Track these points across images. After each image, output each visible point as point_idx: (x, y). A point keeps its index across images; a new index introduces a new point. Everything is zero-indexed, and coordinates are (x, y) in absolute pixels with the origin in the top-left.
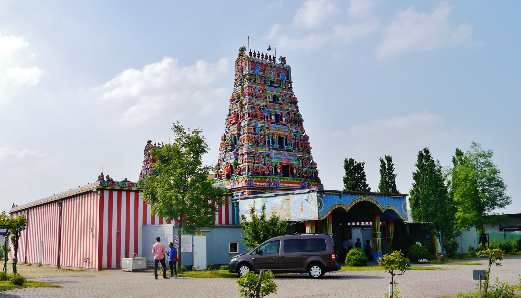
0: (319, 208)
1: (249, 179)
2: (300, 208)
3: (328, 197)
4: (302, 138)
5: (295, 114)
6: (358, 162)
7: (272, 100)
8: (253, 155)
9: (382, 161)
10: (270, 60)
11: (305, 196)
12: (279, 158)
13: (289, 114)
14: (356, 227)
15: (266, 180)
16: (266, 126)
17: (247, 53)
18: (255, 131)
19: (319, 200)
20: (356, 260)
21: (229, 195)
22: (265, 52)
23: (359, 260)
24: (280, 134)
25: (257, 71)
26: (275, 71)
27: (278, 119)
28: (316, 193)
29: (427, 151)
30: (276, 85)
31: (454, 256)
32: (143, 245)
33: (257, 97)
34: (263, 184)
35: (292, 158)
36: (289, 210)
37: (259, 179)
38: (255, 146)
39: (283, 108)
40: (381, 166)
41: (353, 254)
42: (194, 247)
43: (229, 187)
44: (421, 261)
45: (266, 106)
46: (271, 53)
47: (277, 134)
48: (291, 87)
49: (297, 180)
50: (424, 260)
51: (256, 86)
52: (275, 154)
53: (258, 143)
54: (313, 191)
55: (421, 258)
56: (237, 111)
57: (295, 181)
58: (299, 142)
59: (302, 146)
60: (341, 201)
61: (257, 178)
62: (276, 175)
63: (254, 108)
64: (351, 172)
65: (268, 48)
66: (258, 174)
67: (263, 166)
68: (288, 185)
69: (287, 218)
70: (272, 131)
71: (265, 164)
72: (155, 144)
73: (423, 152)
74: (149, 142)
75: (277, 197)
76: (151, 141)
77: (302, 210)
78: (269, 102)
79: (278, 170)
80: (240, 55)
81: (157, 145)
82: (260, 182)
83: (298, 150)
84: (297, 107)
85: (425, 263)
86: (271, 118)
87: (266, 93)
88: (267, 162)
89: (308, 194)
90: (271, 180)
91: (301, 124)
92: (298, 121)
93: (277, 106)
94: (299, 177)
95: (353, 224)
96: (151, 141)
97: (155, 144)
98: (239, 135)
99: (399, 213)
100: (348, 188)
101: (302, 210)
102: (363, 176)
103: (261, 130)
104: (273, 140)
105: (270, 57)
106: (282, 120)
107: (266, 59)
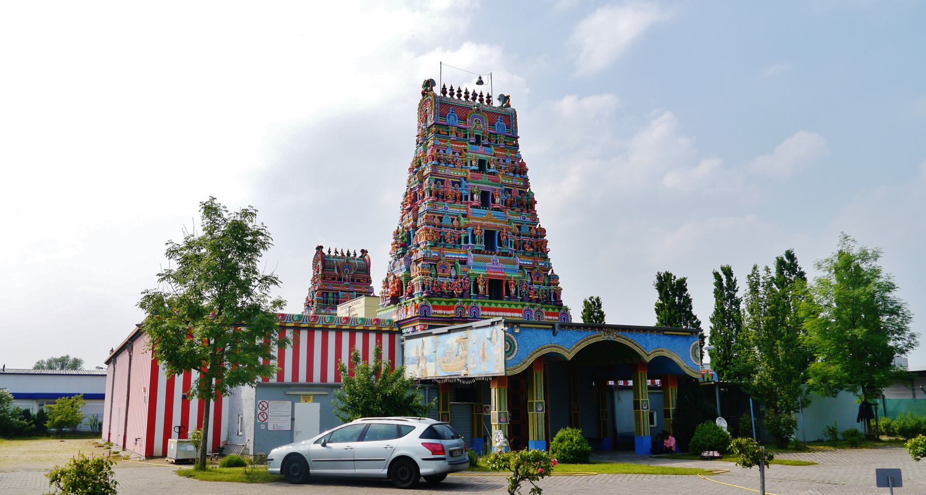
0: (508, 353)
1: (423, 303)
2: (481, 352)
3: (527, 333)
4: (533, 232)
5: (521, 192)
6: (678, 278)
7: (477, 168)
8: (432, 264)
9: (716, 275)
10: (481, 100)
11: (487, 331)
12: (483, 267)
13: (510, 191)
14: (626, 388)
15: (447, 304)
16: (464, 212)
17: (437, 90)
18: (441, 221)
19: (507, 339)
20: (564, 451)
21: (397, 332)
22: (472, 87)
23: (571, 452)
24: (490, 226)
25: (452, 120)
26: (486, 120)
27: (486, 199)
28: (502, 326)
29: (790, 255)
30: (486, 142)
31: (789, 446)
32: (231, 417)
33: (449, 163)
34: (449, 312)
35: (509, 266)
36: (466, 357)
37: (443, 304)
38: (439, 247)
39: (498, 181)
40: (715, 284)
41: (561, 440)
42: (296, 421)
43: (395, 318)
44: (705, 454)
45: (465, 178)
46: (484, 90)
47: (482, 226)
48: (517, 146)
49: (516, 305)
50: (711, 453)
51: (448, 144)
52: (475, 260)
53: (445, 241)
54: (498, 322)
55: (704, 450)
56: (414, 188)
57: (513, 307)
58: (527, 239)
59: (532, 246)
60: (556, 340)
61: (440, 302)
62: (476, 298)
63: (443, 182)
64: (667, 294)
65: (477, 80)
66: (442, 294)
67: (452, 280)
68: (513, 314)
69: (463, 373)
70: (471, 221)
71: (456, 278)
72: (329, 252)
73: (785, 259)
74: (320, 248)
75: (452, 334)
76: (322, 247)
77: (484, 357)
78: (471, 171)
79: (481, 288)
80: (423, 94)
81: (333, 254)
82: (443, 308)
83: (524, 254)
84: (526, 180)
85: (713, 458)
86: (472, 199)
87: (466, 156)
88: (460, 274)
89: (491, 329)
90: (465, 305)
91: (533, 208)
92: (527, 204)
93: (485, 178)
94: (521, 300)
95: (621, 383)
96: (322, 247)
97: (329, 252)
98: (415, 228)
99: (682, 364)
100: (661, 321)
101: (484, 357)
102: (688, 301)
103: (453, 220)
104: (473, 236)
105: (481, 96)
106: (493, 201)
107: (474, 99)
